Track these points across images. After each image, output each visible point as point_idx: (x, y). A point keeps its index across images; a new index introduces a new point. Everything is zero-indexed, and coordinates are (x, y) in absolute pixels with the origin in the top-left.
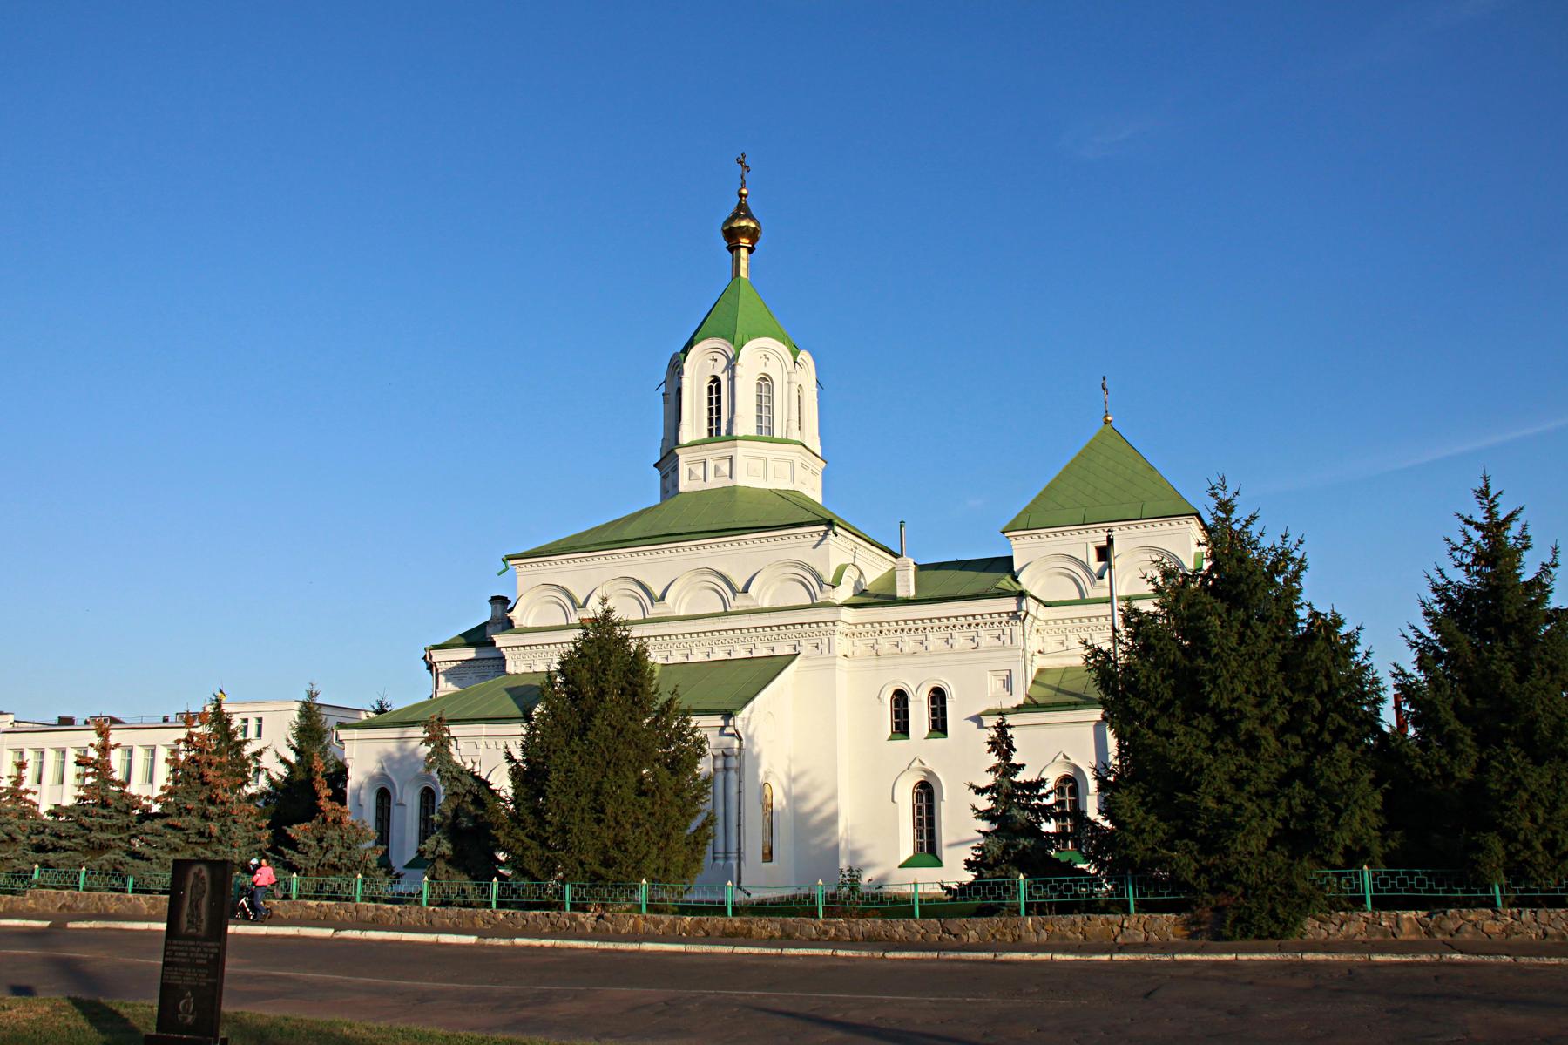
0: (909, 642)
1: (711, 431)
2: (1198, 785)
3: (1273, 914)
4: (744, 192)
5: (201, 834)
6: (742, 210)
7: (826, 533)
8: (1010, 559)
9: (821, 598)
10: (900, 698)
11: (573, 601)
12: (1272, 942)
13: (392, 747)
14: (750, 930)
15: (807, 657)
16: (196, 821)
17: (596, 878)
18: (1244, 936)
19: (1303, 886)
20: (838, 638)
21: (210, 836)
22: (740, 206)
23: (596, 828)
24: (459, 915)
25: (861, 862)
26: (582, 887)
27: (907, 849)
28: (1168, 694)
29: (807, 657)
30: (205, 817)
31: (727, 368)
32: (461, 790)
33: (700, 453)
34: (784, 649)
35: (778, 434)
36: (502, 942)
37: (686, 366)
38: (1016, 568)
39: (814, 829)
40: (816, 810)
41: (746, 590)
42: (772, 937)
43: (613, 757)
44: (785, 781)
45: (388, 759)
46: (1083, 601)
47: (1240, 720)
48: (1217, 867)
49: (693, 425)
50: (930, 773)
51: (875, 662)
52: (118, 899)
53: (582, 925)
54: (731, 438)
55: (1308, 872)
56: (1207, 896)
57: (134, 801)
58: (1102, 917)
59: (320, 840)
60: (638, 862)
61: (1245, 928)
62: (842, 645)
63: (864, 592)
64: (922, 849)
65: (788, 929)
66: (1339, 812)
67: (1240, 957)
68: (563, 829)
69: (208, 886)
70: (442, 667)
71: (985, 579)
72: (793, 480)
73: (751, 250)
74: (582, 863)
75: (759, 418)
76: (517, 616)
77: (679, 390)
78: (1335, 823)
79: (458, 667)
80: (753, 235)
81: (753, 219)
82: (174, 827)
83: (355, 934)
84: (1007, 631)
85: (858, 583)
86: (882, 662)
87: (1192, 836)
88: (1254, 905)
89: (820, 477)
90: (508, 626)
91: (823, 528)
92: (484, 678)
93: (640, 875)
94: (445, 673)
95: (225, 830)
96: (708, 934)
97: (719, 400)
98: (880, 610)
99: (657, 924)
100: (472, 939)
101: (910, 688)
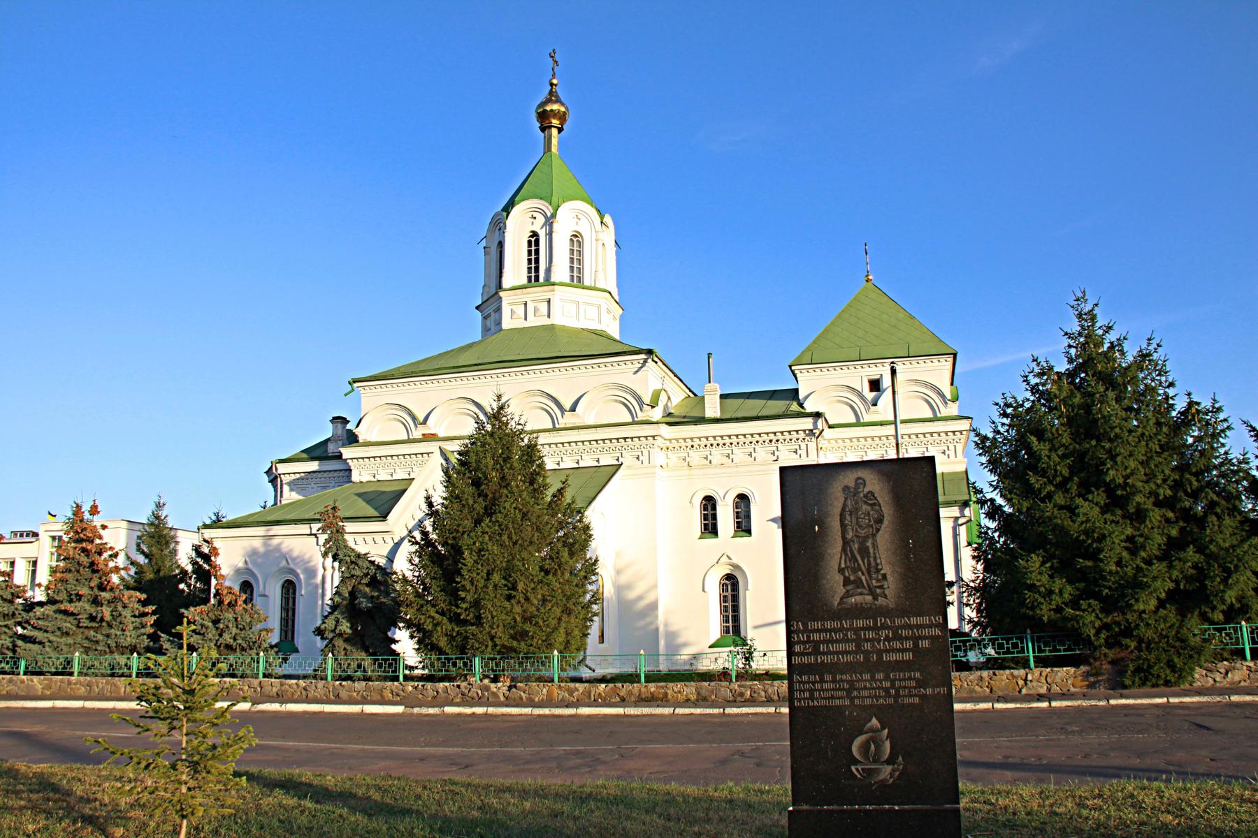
0: (717, 455)
1: (529, 279)
2: (1100, 550)
3: (1171, 666)
4: (555, 81)
5: (92, 618)
6: (552, 97)
7: (645, 361)
8: (796, 391)
9: (641, 416)
10: (709, 503)
11: (414, 418)
12: (1163, 689)
13: (258, 544)
14: (666, 694)
15: (630, 467)
16: (87, 606)
17: (506, 652)
18: (1143, 684)
19: (1195, 641)
20: (656, 452)
21: (102, 620)
22: (551, 93)
23: (507, 604)
24: (367, 689)
25: (680, 640)
26: (493, 659)
27: (715, 632)
28: (1066, 472)
29: (630, 467)
30: (96, 602)
31: (545, 224)
32: (358, 573)
33: (522, 296)
34: (607, 460)
35: (587, 282)
36: (431, 711)
37: (508, 222)
38: (801, 396)
39: (640, 616)
40: (640, 598)
41: (573, 409)
42: (688, 700)
43: (506, 538)
44: (613, 573)
45: (253, 553)
46: (859, 424)
47: (1134, 494)
48: (1118, 624)
49: (515, 271)
50: (736, 567)
51: (687, 472)
52: (10, 681)
53: (495, 694)
54: (548, 282)
55: (1195, 628)
56: (1104, 650)
57: (18, 592)
58: (1007, 672)
59: (216, 622)
60: (549, 635)
61: (1146, 678)
62: (659, 457)
63: (670, 414)
64: (727, 632)
65: (704, 692)
66: (1229, 573)
67: (1172, 700)
68: (476, 604)
69: (887, 511)
70: (286, 479)
71: (777, 406)
72: (600, 322)
73: (560, 130)
74: (492, 638)
75: (572, 269)
76: (363, 433)
77: (501, 245)
78: (1225, 581)
79: (302, 479)
80: (562, 118)
81: (563, 104)
82: (65, 612)
83: (275, 707)
84: (803, 446)
85: (666, 407)
86: (694, 472)
87: (1097, 596)
88: (1152, 657)
89: (618, 322)
90: (352, 439)
91: (643, 356)
92: (325, 488)
93: (550, 646)
94: (289, 484)
95: (116, 616)
96: (623, 700)
97: (537, 252)
98: (693, 427)
99: (571, 692)
100: (400, 709)
101: (717, 494)
